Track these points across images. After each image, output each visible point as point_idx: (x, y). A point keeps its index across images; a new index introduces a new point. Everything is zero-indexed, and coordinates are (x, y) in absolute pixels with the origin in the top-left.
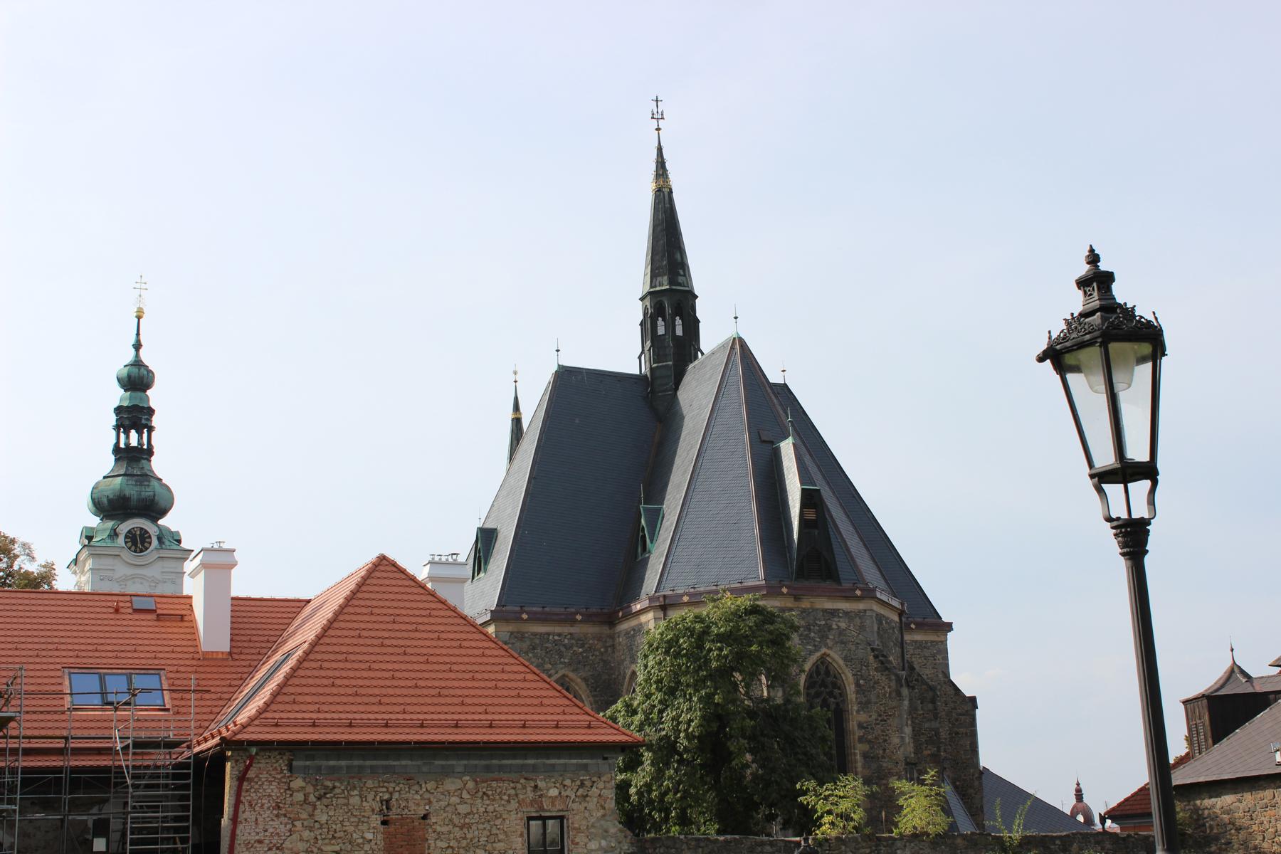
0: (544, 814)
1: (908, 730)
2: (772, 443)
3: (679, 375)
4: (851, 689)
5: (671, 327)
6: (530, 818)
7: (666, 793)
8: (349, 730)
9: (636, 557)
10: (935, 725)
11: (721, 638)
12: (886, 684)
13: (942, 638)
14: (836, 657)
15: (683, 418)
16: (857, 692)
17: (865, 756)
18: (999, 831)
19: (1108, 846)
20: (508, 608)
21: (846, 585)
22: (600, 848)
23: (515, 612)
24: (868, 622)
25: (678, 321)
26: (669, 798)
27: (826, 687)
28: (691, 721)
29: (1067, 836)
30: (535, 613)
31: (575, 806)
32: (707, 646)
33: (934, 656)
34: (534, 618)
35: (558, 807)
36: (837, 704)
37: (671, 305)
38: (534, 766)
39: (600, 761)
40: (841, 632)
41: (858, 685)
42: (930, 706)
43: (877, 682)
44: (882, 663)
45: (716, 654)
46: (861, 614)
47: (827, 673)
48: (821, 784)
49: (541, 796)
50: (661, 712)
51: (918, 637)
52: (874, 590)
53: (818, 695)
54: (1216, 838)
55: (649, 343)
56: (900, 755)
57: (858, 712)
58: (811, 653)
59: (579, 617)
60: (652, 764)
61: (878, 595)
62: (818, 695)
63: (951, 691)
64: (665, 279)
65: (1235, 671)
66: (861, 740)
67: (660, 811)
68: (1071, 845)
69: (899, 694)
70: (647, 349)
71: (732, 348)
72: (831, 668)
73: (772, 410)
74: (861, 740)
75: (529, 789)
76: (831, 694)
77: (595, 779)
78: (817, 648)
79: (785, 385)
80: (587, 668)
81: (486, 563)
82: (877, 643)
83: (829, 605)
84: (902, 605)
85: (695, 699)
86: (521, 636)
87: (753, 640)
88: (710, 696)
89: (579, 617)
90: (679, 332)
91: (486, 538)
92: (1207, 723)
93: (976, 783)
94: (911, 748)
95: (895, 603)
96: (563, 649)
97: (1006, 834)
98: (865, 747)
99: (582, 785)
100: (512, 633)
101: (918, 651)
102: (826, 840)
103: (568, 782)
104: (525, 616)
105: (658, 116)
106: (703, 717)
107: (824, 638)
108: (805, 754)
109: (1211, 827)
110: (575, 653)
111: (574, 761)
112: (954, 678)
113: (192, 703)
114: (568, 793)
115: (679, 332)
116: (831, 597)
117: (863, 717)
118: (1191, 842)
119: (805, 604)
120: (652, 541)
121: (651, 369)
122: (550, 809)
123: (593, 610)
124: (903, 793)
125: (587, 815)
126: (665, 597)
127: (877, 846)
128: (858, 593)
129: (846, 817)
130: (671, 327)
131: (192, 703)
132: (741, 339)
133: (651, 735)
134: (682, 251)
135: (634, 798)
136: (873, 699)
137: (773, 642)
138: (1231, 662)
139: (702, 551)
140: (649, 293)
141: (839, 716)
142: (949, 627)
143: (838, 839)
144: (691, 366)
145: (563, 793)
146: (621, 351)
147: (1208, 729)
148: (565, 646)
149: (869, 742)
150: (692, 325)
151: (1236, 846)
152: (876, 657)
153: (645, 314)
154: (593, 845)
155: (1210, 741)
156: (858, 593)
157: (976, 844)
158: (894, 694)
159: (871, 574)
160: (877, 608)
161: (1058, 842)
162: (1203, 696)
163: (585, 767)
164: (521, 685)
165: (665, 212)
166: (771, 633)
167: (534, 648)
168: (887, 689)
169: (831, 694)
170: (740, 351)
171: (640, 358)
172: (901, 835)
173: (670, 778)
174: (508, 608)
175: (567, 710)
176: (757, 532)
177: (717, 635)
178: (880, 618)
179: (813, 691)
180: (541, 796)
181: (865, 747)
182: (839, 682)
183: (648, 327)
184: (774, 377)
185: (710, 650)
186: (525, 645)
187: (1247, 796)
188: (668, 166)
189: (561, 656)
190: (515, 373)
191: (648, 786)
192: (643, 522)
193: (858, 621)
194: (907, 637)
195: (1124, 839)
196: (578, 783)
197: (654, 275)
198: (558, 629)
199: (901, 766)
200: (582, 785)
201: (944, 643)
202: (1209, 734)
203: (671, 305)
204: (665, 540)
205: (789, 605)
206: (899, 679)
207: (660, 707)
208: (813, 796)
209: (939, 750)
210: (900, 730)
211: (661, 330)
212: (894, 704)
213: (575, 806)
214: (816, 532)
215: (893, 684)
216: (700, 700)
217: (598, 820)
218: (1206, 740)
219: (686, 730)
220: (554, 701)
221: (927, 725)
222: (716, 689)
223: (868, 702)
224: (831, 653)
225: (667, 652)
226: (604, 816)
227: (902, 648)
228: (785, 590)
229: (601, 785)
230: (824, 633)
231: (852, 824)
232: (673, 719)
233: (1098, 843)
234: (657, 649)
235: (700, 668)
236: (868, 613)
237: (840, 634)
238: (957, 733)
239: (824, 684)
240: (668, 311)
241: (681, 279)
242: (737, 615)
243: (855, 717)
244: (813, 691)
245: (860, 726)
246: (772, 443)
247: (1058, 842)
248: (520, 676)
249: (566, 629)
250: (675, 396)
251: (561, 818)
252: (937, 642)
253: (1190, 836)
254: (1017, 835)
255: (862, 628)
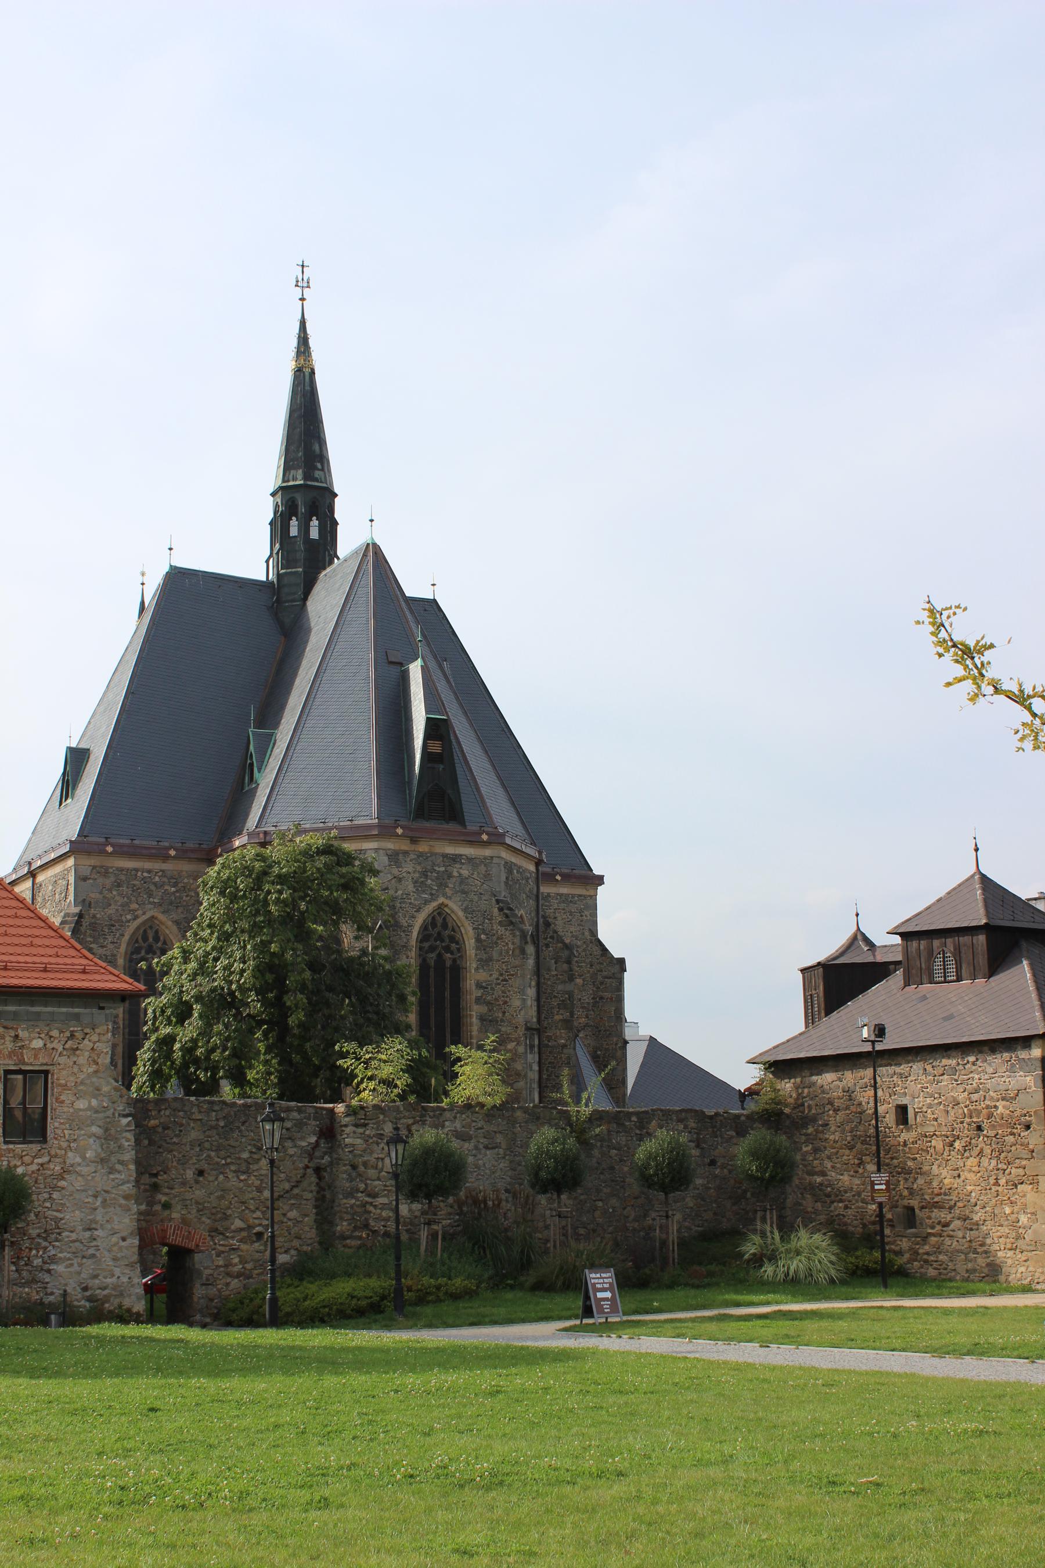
0: (24, 1068)
1: (531, 992)
2: (401, 664)
3: (309, 584)
4: (470, 944)
5: (305, 528)
6: (7, 1072)
7: (213, 1050)
8: (83, 977)
9: (243, 788)
10: (569, 987)
11: (281, 879)
12: (510, 939)
13: (591, 892)
14: (455, 908)
15: (309, 630)
16: (477, 948)
17: (482, 1018)
18: (566, 1104)
19: (692, 1124)
20: (90, 839)
21: (472, 827)
22: (90, 1108)
23: (98, 844)
24: (494, 871)
25: (315, 522)
26: (216, 1056)
27: (442, 941)
28: (243, 971)
29: (646, 1112)
30: (122, 846)
31: (62, 1060)
32: (267, 887)
33: (581, 911)
34: (121, 852)
35: (41, 1060)
36: (454, 960)
37: (305, 500)
38: (15, 1013)
39: (95, 1011)
40: (463, 880)
41: (478, 940)
42: (565, 966)
43: (500, 938)
44: (507, 916)
45: (275, 895)
46: (487, 861)
47: (445, 925)
48: (361, 1046)
49: (22, 1047)
50: (216, 959)
51: (564, 890)
52: (503, 835)
53: (432, 949)
54: (814, 1119)
55: (277, 546)
56: (520, 1019)
57: (477, 969)
58: (426, 902)
59: (172, 853)
60: (201, 1016)
61: (508, 841)
62: (432, 949)
63: (597, 951)
64: (300, 473)
65: (859, 938)
66: (478, 1000)
67: (206, 1070)
68: (649, 1123)
69: (523, 951)
70: (275, 551)
71: (365, 555)
72: (448, 919)
73: (412, 628)
74: (478, 1000)
75: (8, 1038)
76: (447, 949)
77: (87, 1030)
78: (433, 897)
79: (435, 600)
80: (180, 910)
81: (74, 787)
82: (503, 894)
83: (450, 850)
84: (540, 853)
85: (249, 947)
86: (105, 872)
87: (327, 880)
88: (265, 944)
89: (172, 853)
90: (314, 534)
91: (76, 758)
92: (821, 994)
93: (619, 1053)
94: (533, 1012)
95: (532, 851)
96: (153, 887)
97: (572, 1109)
98: (484, 1009)
99: (72, 1036)
100: (94, 867)
101: (563, 905)
102: (362, 1108)
103: (55, 1033)
104: (110, 849)
105: (303, 284)
106: (257, 968)
107: (442, 885)
108: (377, 1013)
109: (809, 1106)
110: (166, 892)
111: (64, 1010)
112: (602, 936)
113: (893, 987)
114: (55, 1045)
115: (314, 534)
116: (453, 841)
117: (483, 976)
118: (788, 1123)
119: (423, 847)
120: (259, 770)
121: (278, 575)
122: (32, 1063)
123: (190, 845)
124: (459, 1059)
125: (75, 1070)
126: (266, 833)
127: (422, 1116)
128: (485, 837)
129: (389, 1083)
130: (305, 528)
131: (893, 987)
132: (375, 545)
133: (205, 985)
134: (322, 442)
135: (177, 1055)
136: (495, 956)
137: (345, 887)
138: (855, 928)
139: (316, 781)
140: (281, 488)
141: (457, 972)
142: (600, 880)
143: (375, 1106)
144: (324, 573)
145: (49, 1046)
146: (243, 549)
147: (822, 1000)
148: (155, 884)
149: (488, 1003)
150: (330, 527)
151: (833, 1128)
152: (501, 910)
153: (275, 513)
154: (81, 1104)
155: (823, 1014)
156: (485, 837)
157: (538, 1118)
158: (517, 952)
159: (502, 813)
160: (505, 854)
161: (634, 1119)
162: (819, 964)
163: (77, 1017)
164: (11, 922)
165: (304, 396)
166: (342, 876)
167: (119, 885)
168: (511, 946)
169: (447, 949)
170: (374, 557)
171: (267, 562)
172: (452, 1106)
173: (219, 1033)
174: (90, 839)
175: (61, 952)
176: (374, 764)
177: (279, 876)
178: (509, 867)
179: (426, 945)
180: (22, 1047)
181: (484, 1009)
182: (458, 936)
183: (279, 526)
184: (413, 587)
185: (269, 892)
186: (109, 881)
187: (848, 1074)
188: (311, 342)
189: (150, 896)
190: (143, 574)
191: (194, 1041)
192: (252, 748)
193: (482, 868)
194: (544, 889)
195: (711, 1117)
196: (68, 1034)
197: (288, 466)
198: (148, 865)
199: (521, 1031)
200: (72, 1036)
201: (594, 897)
202: (823, 1006)
203: (305, 500)
204: (272, 770)
205: (404, 848)
206: (524, 935)
207: (214, 954)
208: (351, 1057)
209: (572, 1014)
210: (522, 992)
211: (294, 531)
212: (517, 963)
213: (62, 1060)
214: (441, 767)
215: (517, 940)
216: (254, 948)
217: (89, 1076)
218: (819, 1011)
219: (238, 981)
220: (47, 942)
221: (560, 987)
222: (273, 937)
223: (490, 959)
224: (451, 904)
225: (222, 893)
226: (96, 1072)
227: (538, 901)
228: (400, 831)
229: (95, 1038)
230: (442, 881)
231: (396, 1091)
232: (225, 969)
233: (680, 1121)
234: (212, 888)
235: (258, 912)
236: (495, 860)
237: (461, 883)
238: (601, 998)
239: (440, 937)
240: (302, 509)
241: (318, 474)
242: (307, 854)
243: (473, 976)
244: (426, 945)
245: (479, 986)
246: (401, 664)
247: (634, 1119)
248: (11, 912)
249: (157, 865)
250: (304, 604)
251: (46, 1073)
252: (585, 897)
253: (788, 1116)
254: (585, 1111)
255: (487, 876)
